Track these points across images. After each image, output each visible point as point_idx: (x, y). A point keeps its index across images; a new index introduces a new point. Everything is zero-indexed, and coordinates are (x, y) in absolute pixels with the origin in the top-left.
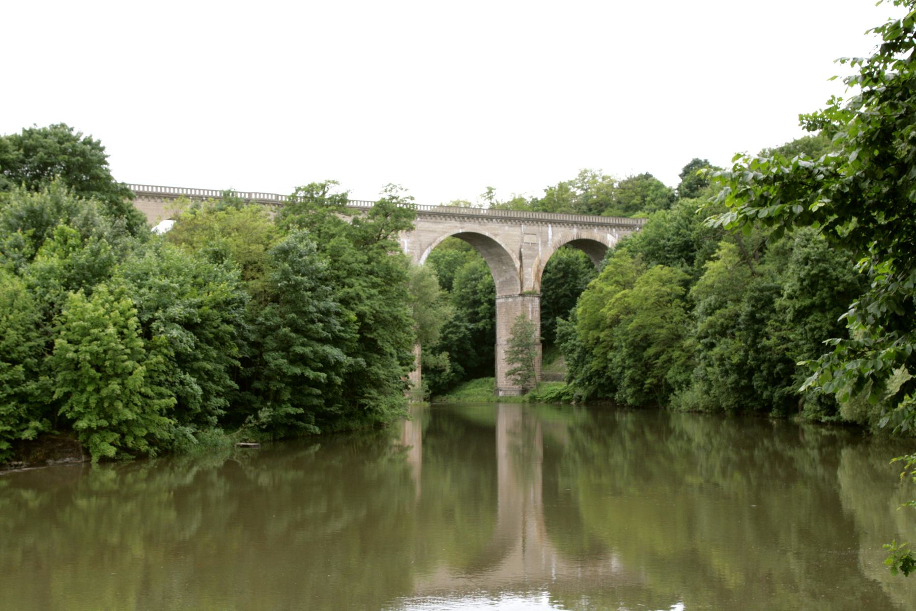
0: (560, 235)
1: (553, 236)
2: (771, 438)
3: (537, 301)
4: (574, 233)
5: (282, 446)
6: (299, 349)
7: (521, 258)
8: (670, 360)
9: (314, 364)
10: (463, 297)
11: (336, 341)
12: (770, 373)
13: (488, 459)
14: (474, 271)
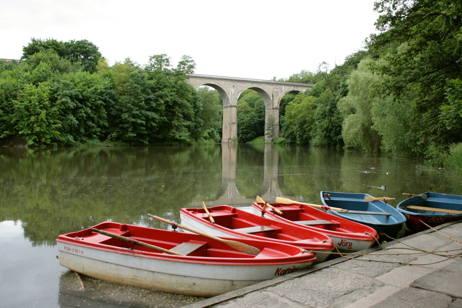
0: (287, 89)
3: (278, 111)
4: (292, 89)
5: (133, 148)
6: (134, 112)
7: (273, 96)
8: (311, 129)
9: (142, 118)
10: (257, 110)
11: (155, 110)
12: (336, 131)
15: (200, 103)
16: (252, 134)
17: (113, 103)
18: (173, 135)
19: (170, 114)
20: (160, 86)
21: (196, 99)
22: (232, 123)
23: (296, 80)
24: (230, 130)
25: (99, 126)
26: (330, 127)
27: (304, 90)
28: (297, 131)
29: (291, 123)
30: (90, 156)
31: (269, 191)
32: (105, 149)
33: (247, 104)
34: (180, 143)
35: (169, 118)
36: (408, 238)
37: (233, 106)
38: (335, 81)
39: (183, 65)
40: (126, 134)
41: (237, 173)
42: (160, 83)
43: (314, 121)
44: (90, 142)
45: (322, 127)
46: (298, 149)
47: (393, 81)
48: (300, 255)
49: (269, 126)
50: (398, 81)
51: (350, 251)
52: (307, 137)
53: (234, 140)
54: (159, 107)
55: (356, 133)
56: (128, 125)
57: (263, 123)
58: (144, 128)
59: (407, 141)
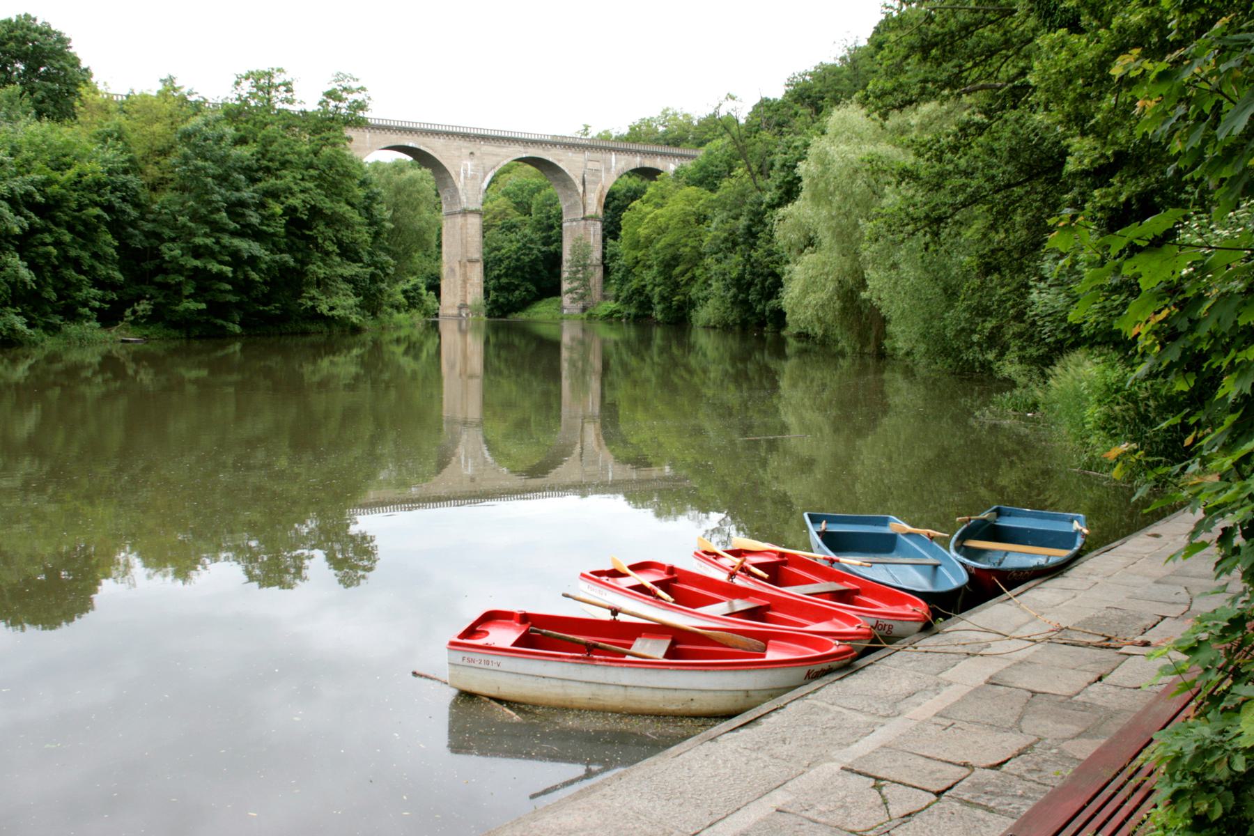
1: (616, 163)
2: (762, 350)
3: (599, 225)
4: (637, 162)
5: (196, 344)
6: (199, 240)
7: (584, 184)
8: (693, 278)
10: (539, 222)
11: (257, 235)
12: (763, 287)
13: (554, 374)
14: (550, 197)
15: (384, 207)
16: (527, 290)
17: (134, 213)
18: (310, 303)
19: (301, 244)
20: (270, 164)
21: (372, 198)
22: (470, 261)
23: (647, 134)
24: (465, 282)
25: (99, 283)
26: (747, 277)
27: (670, 166)
28: (655, 285)
29: (638, 262)
30: (73, 371)
31: (578, 449)
32: (118, 351)
33: (509, 203)
34: (328, 326)
35: (299, 256)
36: (975, 612)
37: (472, 212)
38: (759, 147)
39: (334, 99)
40: (178, 305)
41: (486, 404)
42: (269, 155)
43: (701, 256)
44: (73, 329)
45: (725, 274)
46: (658, 334)
47: (925, 204)
48: (833, 650)
49: (574, 269)
50: (937, 204)
51: (891, 639)
52: (684, 302)
53: (476, 311)
54: (268, 226)
55: (823, 306)
56: (181, 278)
57: (554, 260)
58: (229, 287)
59: (950, 333)
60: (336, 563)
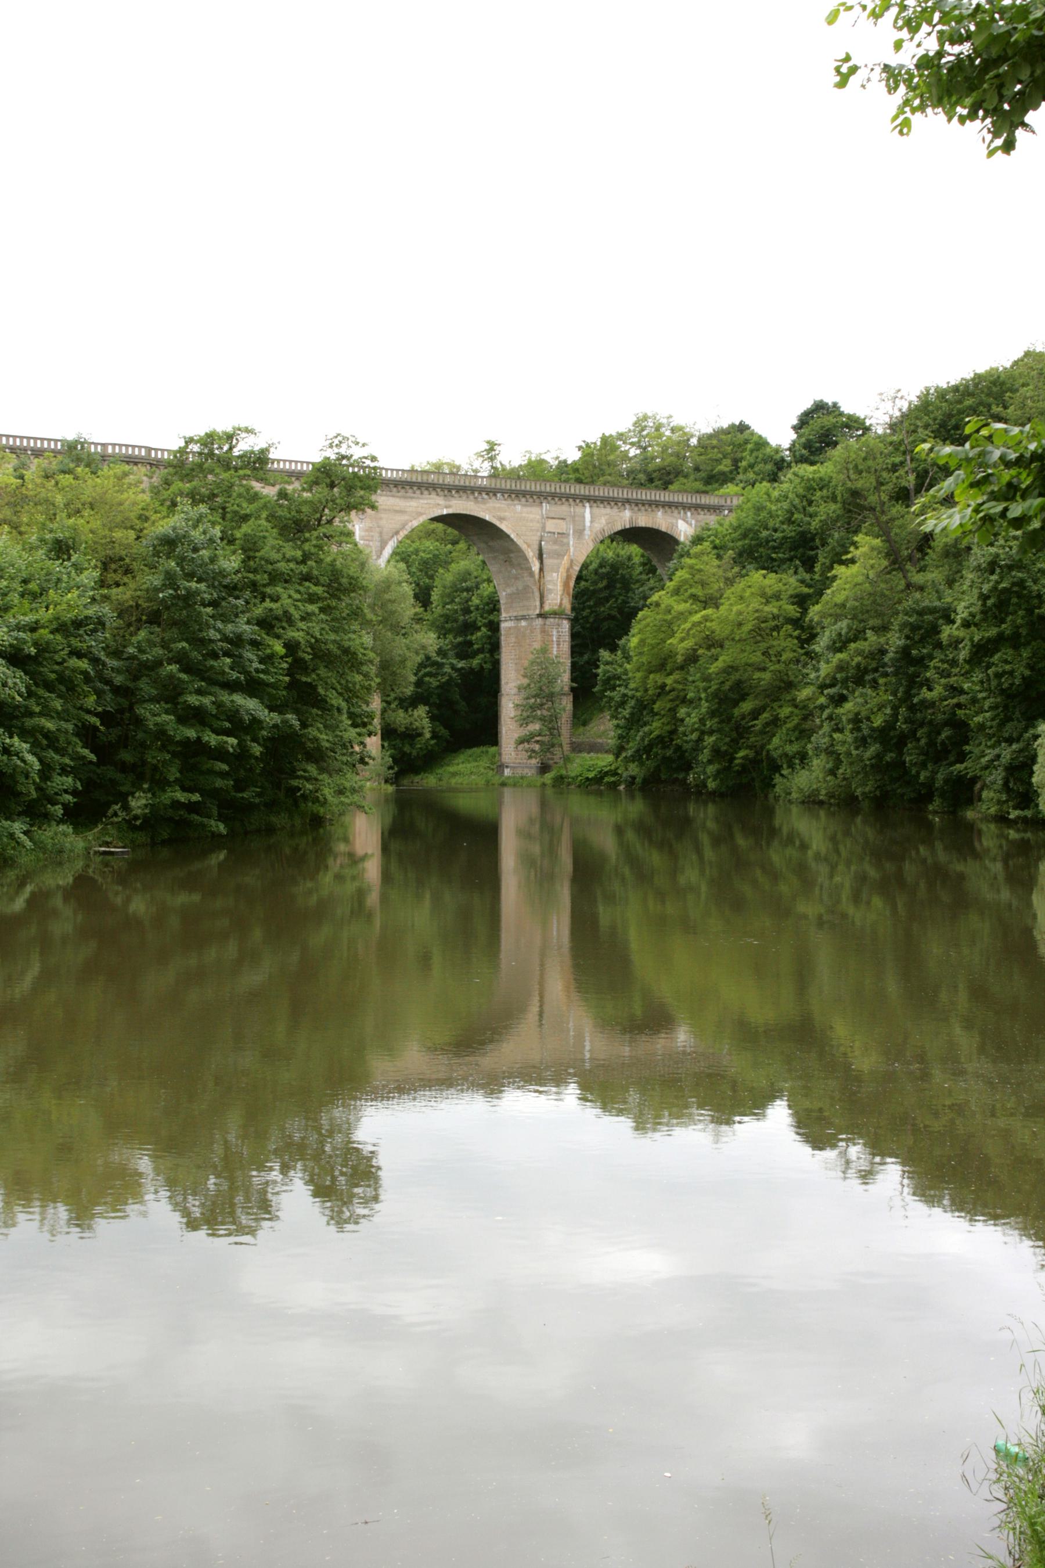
0: (603, 521)
1: (591, 522)
3: (566, 625)
4: (625, 518)
5: (165, 853)
6: (193, 700)
9: (217, 724)
10: (447, 618)
11: (252, 687)
12: (931, 743)
58: (225, 767)
60: (322, 1191)
